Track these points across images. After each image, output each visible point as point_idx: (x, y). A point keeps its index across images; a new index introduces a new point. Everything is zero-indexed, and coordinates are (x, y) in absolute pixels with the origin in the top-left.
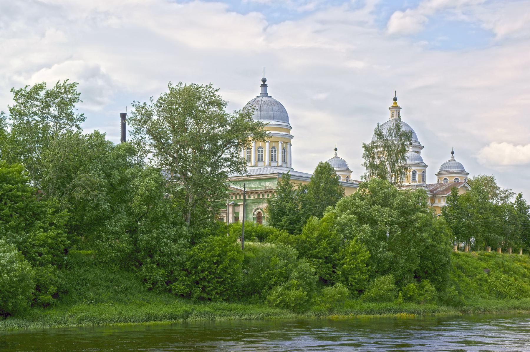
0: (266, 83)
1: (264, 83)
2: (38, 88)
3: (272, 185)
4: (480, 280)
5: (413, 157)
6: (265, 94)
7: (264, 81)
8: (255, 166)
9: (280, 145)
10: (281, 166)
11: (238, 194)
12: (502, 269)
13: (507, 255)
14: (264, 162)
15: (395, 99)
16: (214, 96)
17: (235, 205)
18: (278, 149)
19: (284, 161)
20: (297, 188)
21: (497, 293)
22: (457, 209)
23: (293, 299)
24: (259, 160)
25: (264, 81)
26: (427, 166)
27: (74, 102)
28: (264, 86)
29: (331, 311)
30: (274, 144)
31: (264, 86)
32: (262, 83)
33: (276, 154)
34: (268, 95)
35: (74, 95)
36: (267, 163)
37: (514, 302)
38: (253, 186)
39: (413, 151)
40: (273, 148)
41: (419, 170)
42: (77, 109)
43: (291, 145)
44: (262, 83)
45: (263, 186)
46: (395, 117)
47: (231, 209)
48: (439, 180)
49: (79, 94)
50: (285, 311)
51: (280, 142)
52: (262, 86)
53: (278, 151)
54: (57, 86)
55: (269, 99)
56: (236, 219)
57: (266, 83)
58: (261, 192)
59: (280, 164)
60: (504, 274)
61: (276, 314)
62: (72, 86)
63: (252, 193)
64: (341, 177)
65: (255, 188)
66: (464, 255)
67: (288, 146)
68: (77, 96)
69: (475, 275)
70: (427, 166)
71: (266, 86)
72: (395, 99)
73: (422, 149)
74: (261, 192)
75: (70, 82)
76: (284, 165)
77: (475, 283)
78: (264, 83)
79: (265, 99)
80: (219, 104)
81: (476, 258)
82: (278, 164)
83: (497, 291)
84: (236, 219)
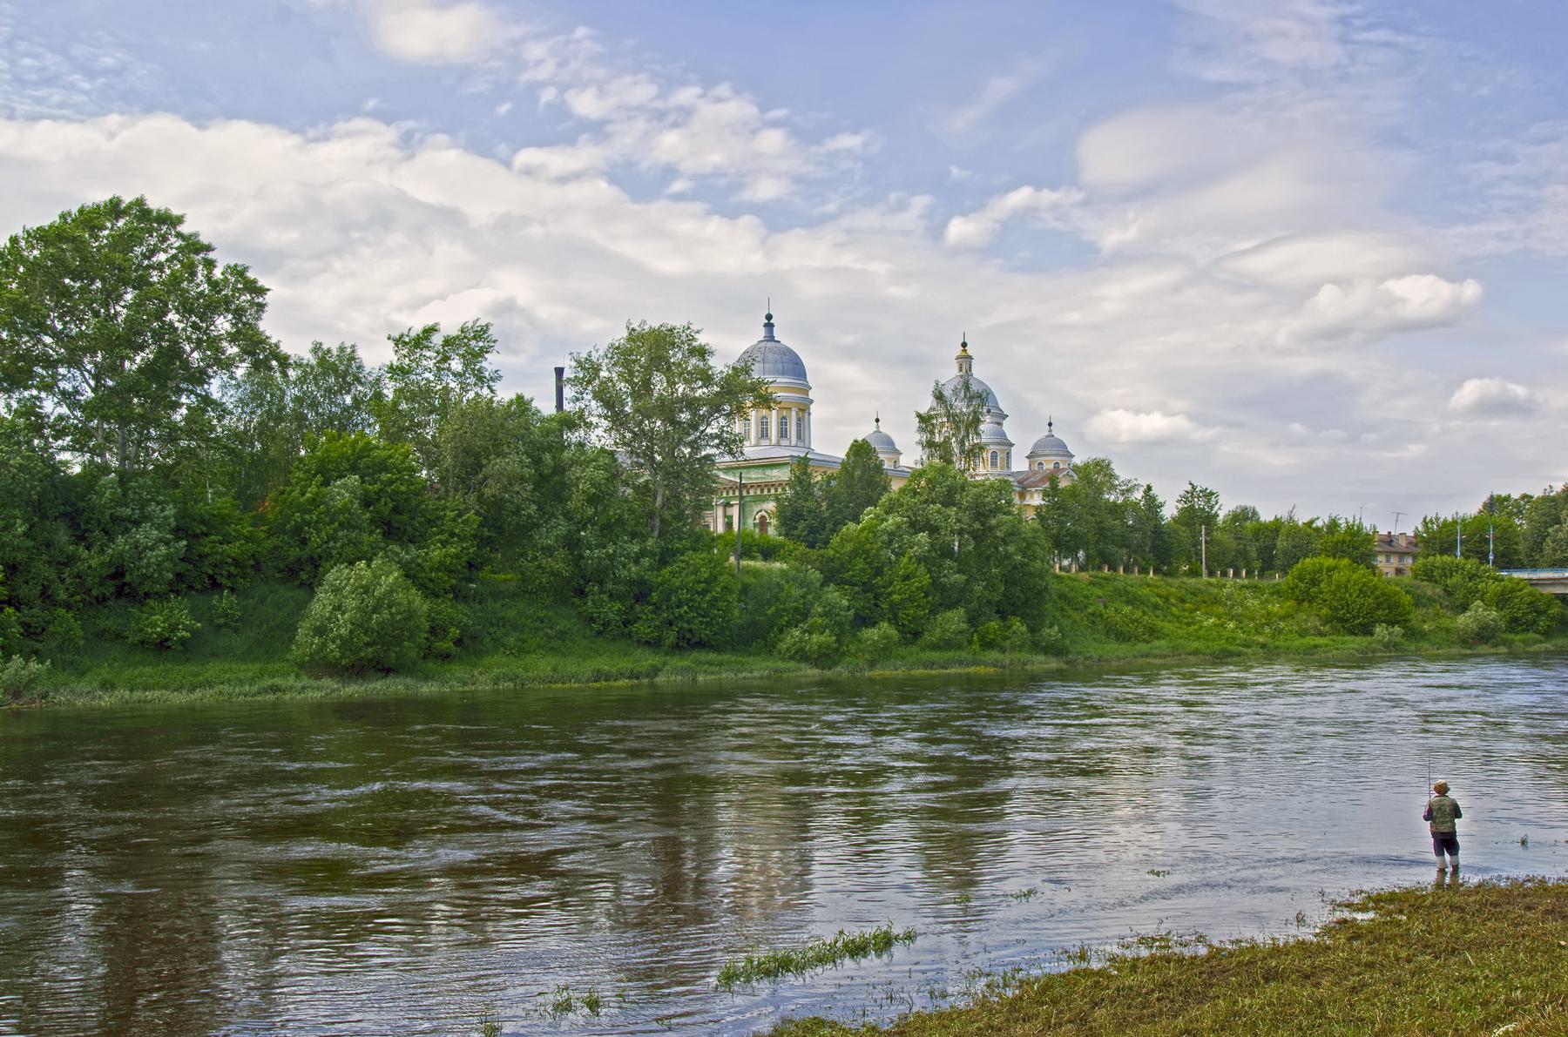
4: (1093, 614)
7: (769, 317)
9: (794, 413)
11: (731, 488)
12: (1124, 598)
19: (799, 437)
25: (769, 317)
27: (487, 352)
28: (769, 326)
31: (769, 326)
38: (753, 476)
40: (784, 418)
42: (490, 363)
49: (495, 341)
52: (765, 325)
55: (777, 344)
56: (729, 525)
58: (780, 485)
59: (794, 443)
63: (752, 487)
65: (757, 478)
66: (1069, 578)
69: (1086, 607)
74: (780, 485)
84: (729, 525)
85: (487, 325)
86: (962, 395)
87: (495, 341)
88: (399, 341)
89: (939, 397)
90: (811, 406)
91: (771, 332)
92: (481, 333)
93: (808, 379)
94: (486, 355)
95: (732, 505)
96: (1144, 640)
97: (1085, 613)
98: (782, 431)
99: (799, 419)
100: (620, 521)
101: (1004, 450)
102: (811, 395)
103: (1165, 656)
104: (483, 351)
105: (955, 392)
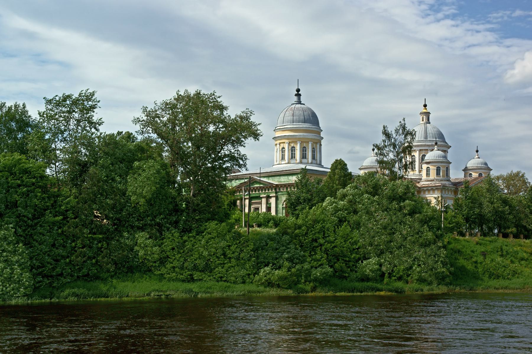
0: (299, 93)
1: (298, 93)
2: (66, 98)
3: (293, 179)
4: (476, 262)
5: (437, 155)
6: (299, 102)
7: (298, 90)
8: (289, 163)
9: (310, 145)
10: (312, 163)
11: (270, 187)
12: (500, 253)
13: (507, 240)
14: (296, 160)
15: (425, 106)
16: (217, 101)
17: (268, 198)
18: (308, 148)
19: (314, 158)
20: (313, 181)
21: (490, 275)
22: (468, 199)
23: (277, 278)
24: (292, 158)
25: (298, 90)
26: (450, 163)
27: (94, 108)
28: (298, 95)
29: (314, 289)
30: (305, 145)
31: (298, 95)
32: (297, 93)
33: (307, 152)
34: (302, 103)
35: (95, 102)
36: (298, 161)
37: (506, 283)
38: (283, 180)
39: (438, 150)
40: (305, 147)
41: (443, 166)
42: (96, 116)
43: (321, 145)
44: (297, 93)
45: (290, 180)
46: (425, 121)
47: (264, 201)
48: (465, 175)
49: (99, 102)
50: (268, 289)
51: (298, 142)
52: (296, 95)
53: (308, 150)
54: (80, 95)
55: (302, 106)
56: (269, 209)
57: (299, 93)
58: (289, 186)
59: (310, 161)
60: (331, 268)
61: (259, 292)
62: (93, 94)
63: (281, 186)
64: (483, 175)
65: (284, 181)
66: (465, 240)
67: (318, 146)
68: (96, 103)
69: (472, 257)
70: (450, 163)
71: (300, 95)
72: (425, 106)
73: (449, 148)
74: (289, 186)
75: (91, 91)
76: (314, 161)
77: (470, 265)
78: (298, 93)
79: (299, 105)
80: (222, 108)
81: (475, 243)
82: (308, 161)
83: (491, 272)
84: (269, 209)
85: (93, 92)
86: (401, 131)
87: (99, 102)
88: (49, 102)
89: (387, 135)
90: (322, 141)
91: (299, 99)
92: (89, 97)
93: (320, 126)
94: (94, 110)
95: (271, 197)
96: (508, 278)
97: (470, 261)
98: (303, 155)
99: (313, 148)
100: (143, 198)
101: (445, 166)
102: (322, 134)
103: (517, 289)
104: (93, 107)
105: (397, 131)
